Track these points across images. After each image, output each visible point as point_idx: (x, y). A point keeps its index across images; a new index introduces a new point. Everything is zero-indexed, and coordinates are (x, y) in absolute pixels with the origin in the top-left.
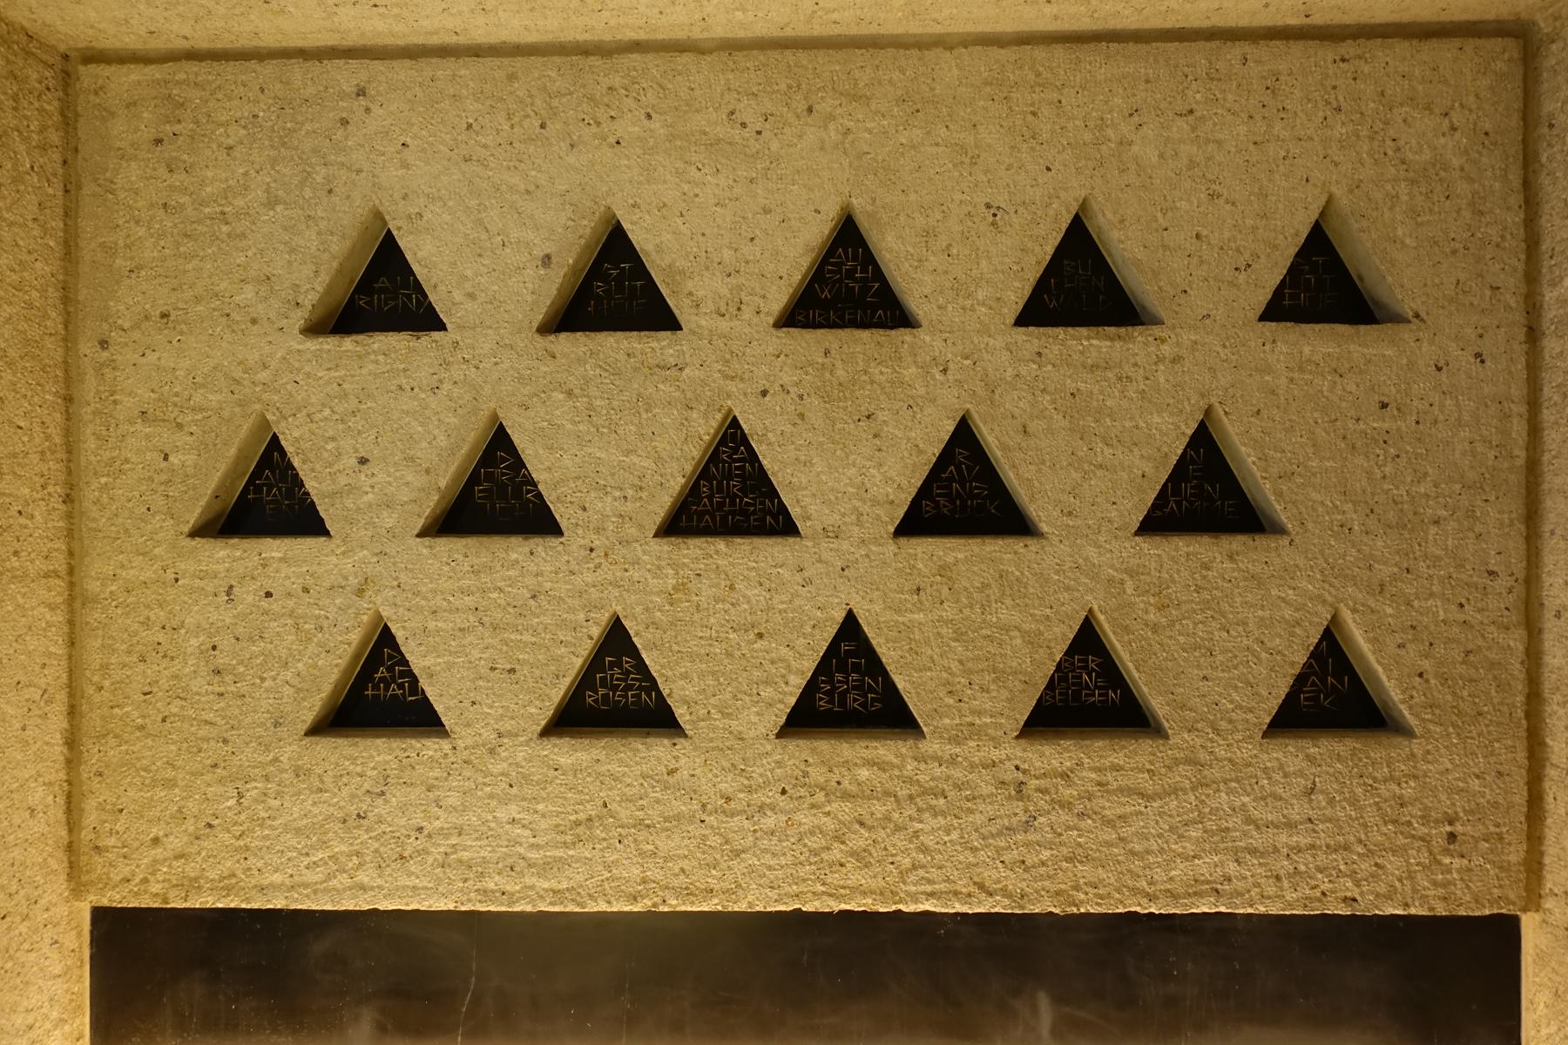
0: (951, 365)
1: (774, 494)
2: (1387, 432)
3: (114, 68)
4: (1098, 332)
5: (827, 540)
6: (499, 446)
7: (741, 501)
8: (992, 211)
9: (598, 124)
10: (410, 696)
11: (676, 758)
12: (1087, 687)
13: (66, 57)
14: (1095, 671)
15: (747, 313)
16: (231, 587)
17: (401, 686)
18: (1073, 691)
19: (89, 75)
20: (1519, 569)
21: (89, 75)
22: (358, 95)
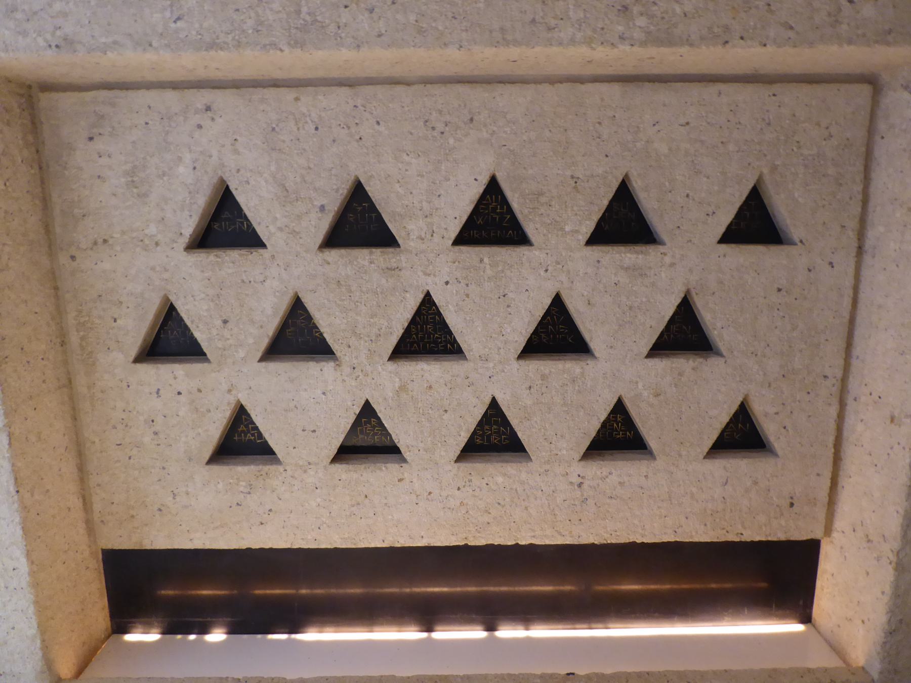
0: (550, 268)
1: (450, 333)
2: (780, 304)
3: (61, 94)
4: (630, 249)
5: (482, 362)
6: (297, 308)
7: (434, 336)
8: (575, 180)
9: (349, 128)
10: (258, 440)
11: (403, 474)
12: (617, 431)
13: (30, 87)
14: (621, 422)
15: (436, 238)
16: (159, 390)
17: (253, 435)
18: (609, 432)
19: (45, 100)
20: (839, 374)
21: (45, 100)
22: (207, 110)
